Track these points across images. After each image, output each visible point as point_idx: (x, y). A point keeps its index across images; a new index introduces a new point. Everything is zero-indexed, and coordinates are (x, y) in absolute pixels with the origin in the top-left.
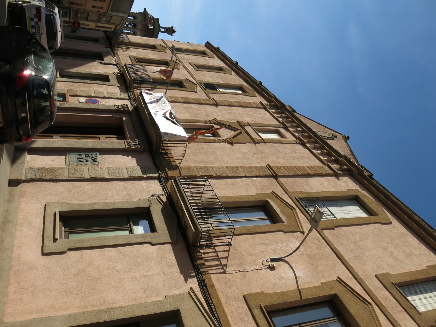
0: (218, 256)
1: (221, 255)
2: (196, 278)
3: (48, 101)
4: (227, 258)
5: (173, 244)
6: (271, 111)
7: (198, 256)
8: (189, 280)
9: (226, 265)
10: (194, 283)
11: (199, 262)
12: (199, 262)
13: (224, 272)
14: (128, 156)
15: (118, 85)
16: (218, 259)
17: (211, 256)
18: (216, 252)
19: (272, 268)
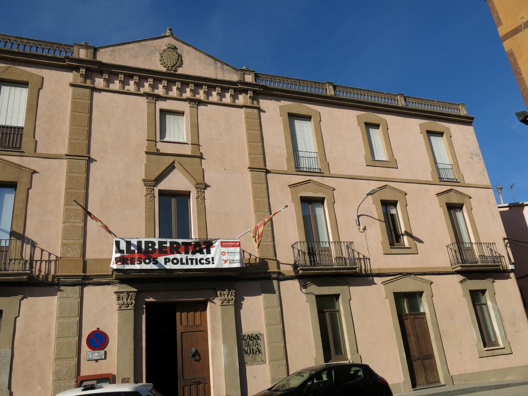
0: (46, 261)
1: (46, 257)
2: (374, 278)
3: (327, 378)
4: (50, 254)
5: (350, 285)
6: (112, 87)
7: (43, 278)
8: (511, 276)
9: (364, 256)
10: (376, 279)
11: (50, 279)
12: (50, 279)
13: (369, 259)
14: (242, 304)
15: (20, 297)
16: (50, 261)
17: (44, 267)
18: (41, 261)
19: (365, 229)
